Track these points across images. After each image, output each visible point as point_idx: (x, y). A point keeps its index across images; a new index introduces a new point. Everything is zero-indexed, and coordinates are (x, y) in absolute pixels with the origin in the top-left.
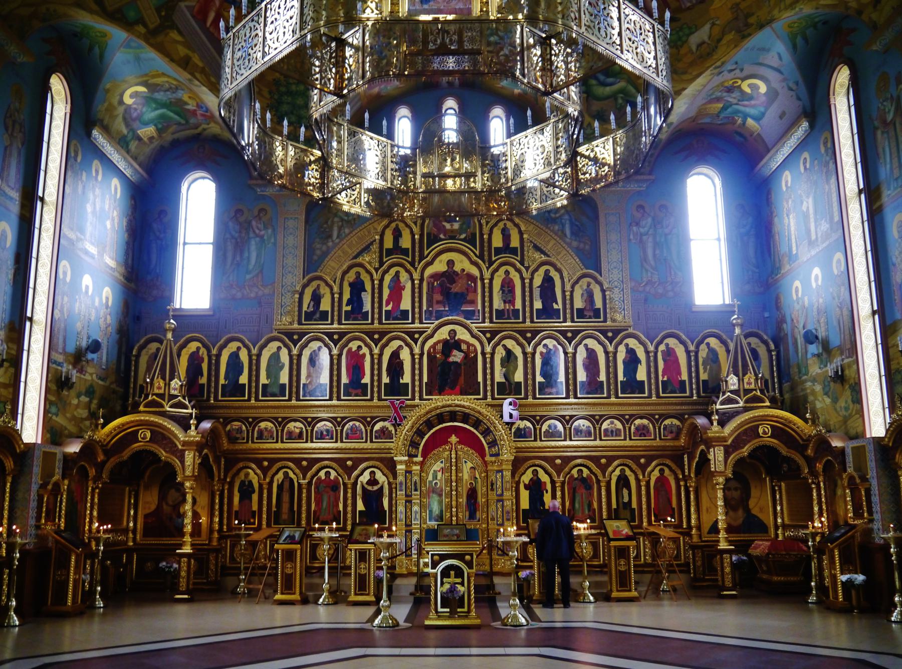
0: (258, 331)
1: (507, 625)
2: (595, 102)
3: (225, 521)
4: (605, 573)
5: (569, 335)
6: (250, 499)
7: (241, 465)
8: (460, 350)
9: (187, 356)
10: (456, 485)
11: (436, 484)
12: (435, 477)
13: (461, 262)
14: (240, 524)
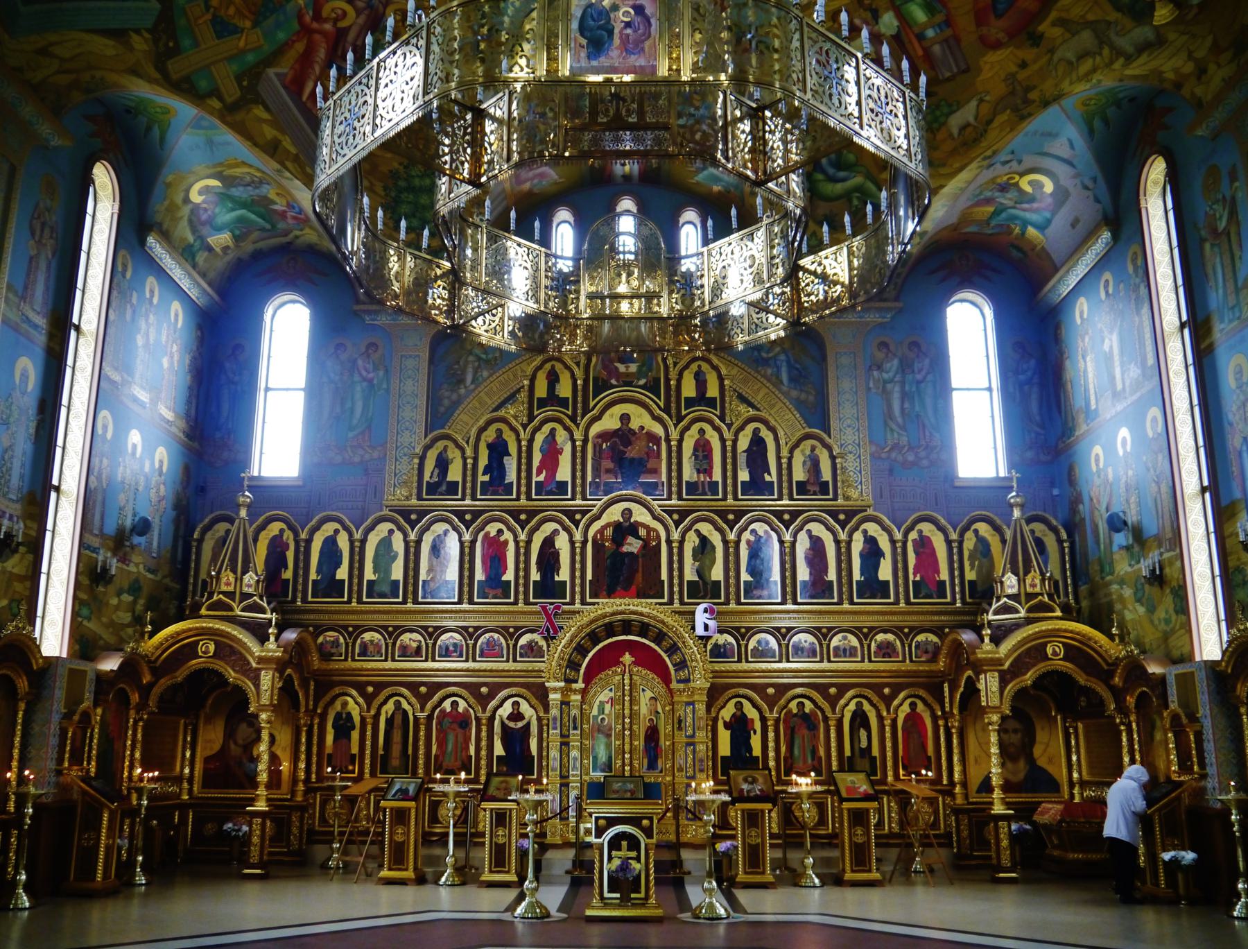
0: (363, 509)
1: (699, 918)
2: (822, 204)
3: (314, 768)
4: (836, 846)
5: (786, 517)
7: (337, 690)
8: (638, 537)
9: (267, 542)
10: (631, 723)
11: (603, 719)
12: (601, 711)
13: (640, 416)
14: (334, 772)
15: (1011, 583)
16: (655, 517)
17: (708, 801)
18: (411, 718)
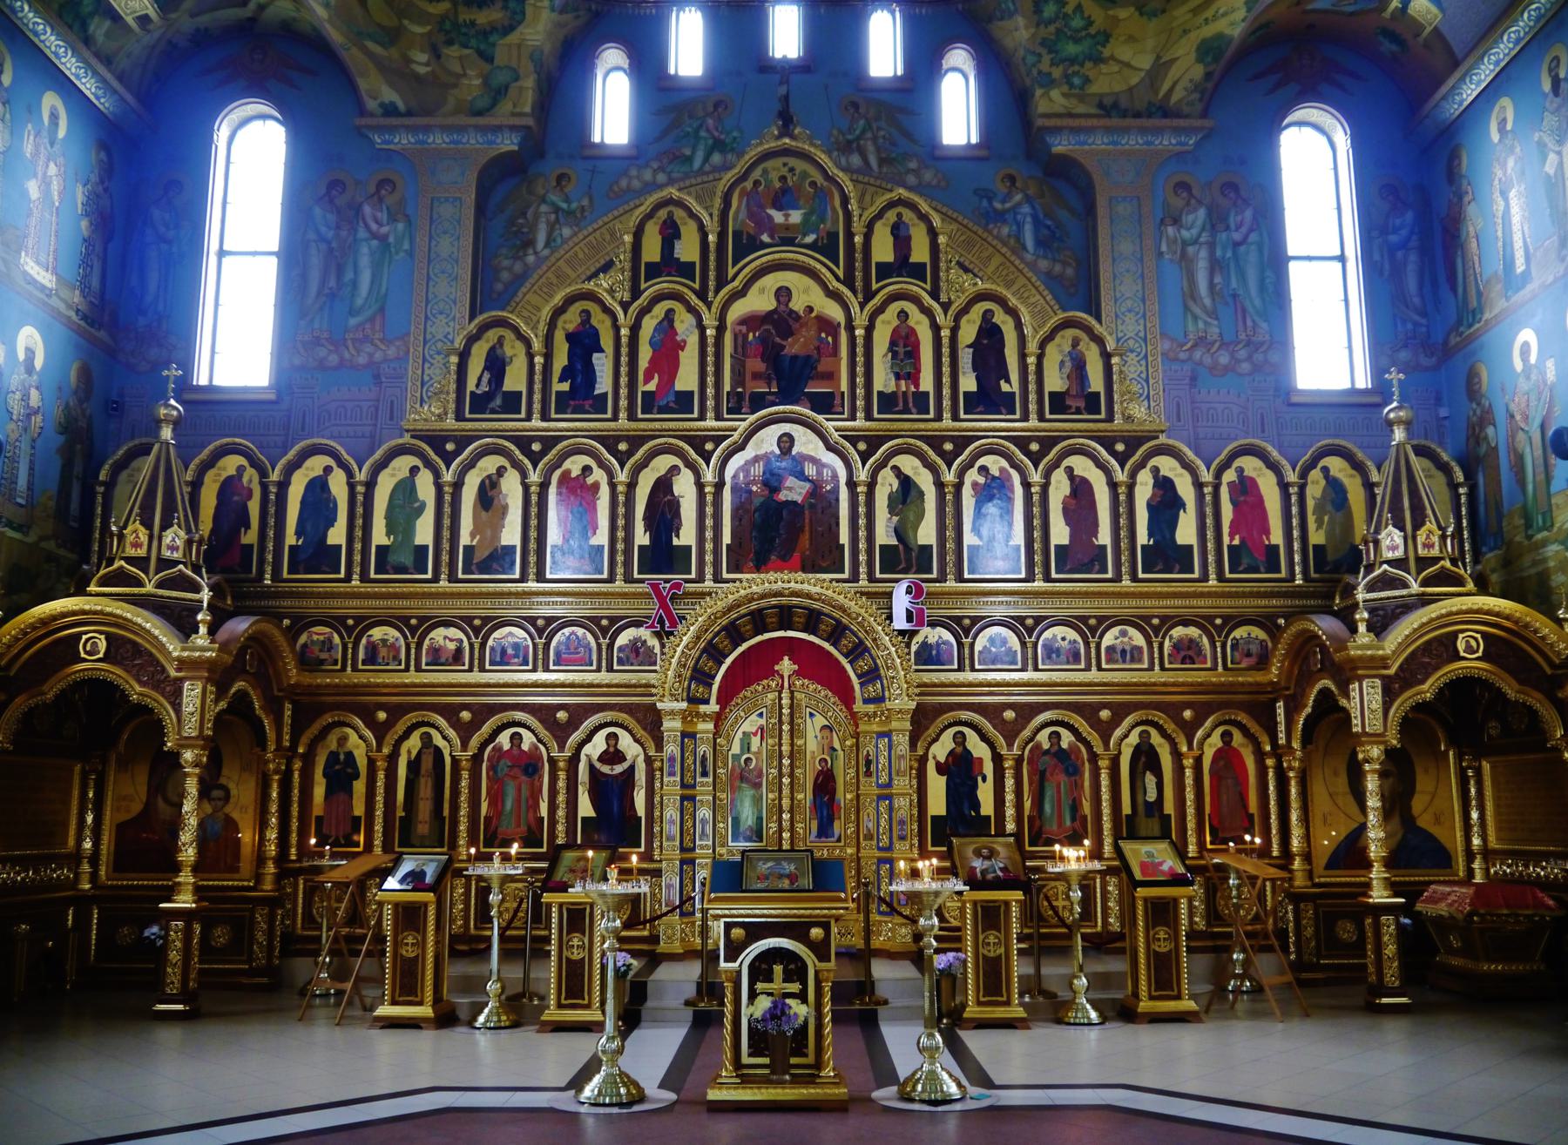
0: (372, 436)
1: (912, 1100)
3: (294, 838)
4: (1122, 951)
5: (1034, 447)
6: (349, 792)
7: (328, 719)
9: (216, 487)
10: (792, 765)
11: (748, 760)
12: (746, 747)
13: (806, 291)
14: (320, 844)
15: (1392, 541)
16: (830, 448)
17: (928, 893)
18: (448, 760)
